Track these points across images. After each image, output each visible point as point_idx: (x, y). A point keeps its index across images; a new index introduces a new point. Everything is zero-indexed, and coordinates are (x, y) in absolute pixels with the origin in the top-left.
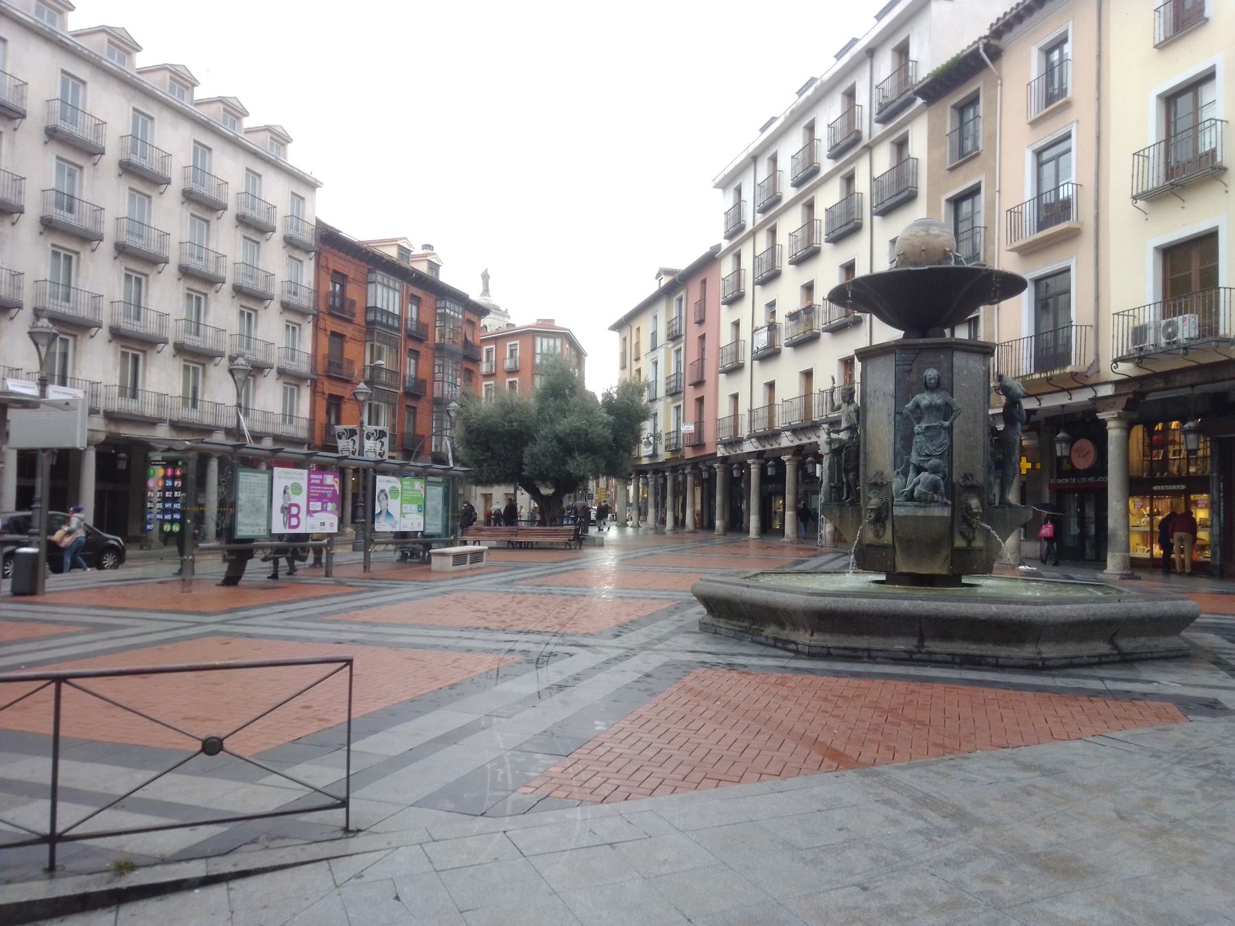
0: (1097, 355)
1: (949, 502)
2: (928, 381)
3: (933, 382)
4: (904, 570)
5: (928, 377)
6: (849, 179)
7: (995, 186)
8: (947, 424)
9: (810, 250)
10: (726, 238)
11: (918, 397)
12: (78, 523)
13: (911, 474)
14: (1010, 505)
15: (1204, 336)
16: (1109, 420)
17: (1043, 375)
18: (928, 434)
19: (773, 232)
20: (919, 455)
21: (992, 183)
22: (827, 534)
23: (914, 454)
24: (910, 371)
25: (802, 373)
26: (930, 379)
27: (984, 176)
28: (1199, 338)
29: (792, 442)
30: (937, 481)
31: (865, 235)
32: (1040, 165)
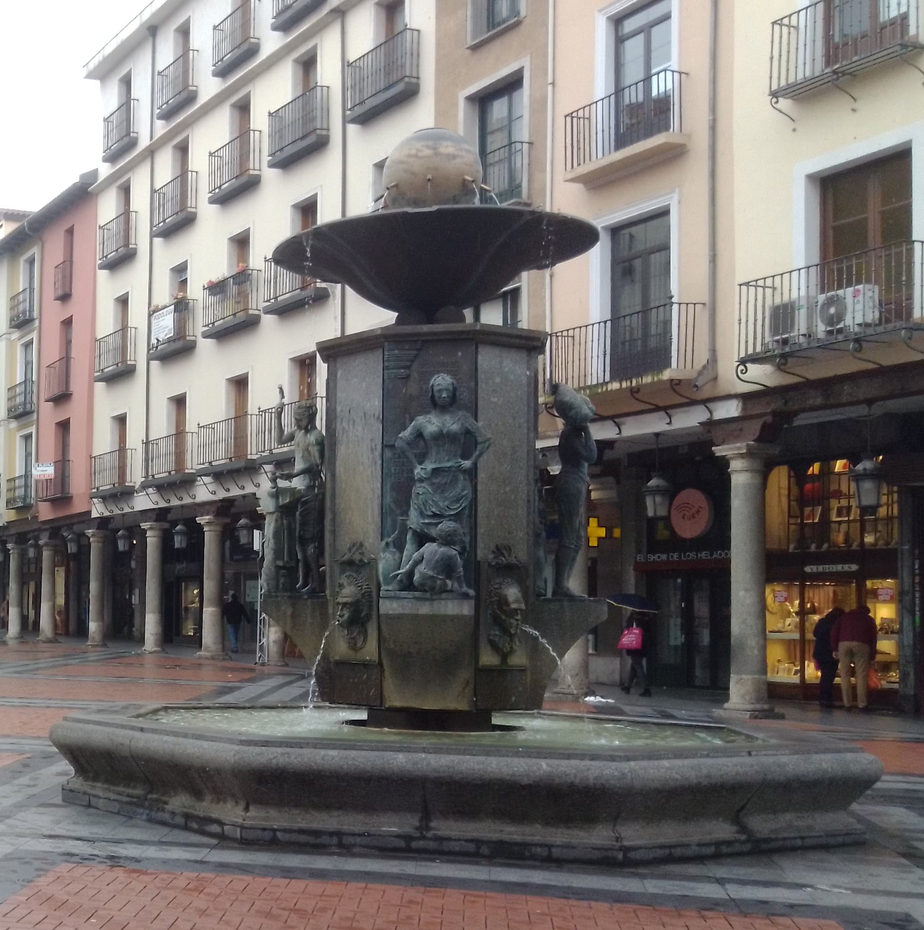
0: (713, 351)
1: (472, 592)
2: (436, 395)
4: (398, 704)
5: (436, 388)
6: (308, 64)
7: (546, 74)
8: (467, 464)
9: (244, 179)
10: (105, 160)
11: (420, 420)
13: (409, 546)
14: (571, 598)
15: (888, 321)
16: (733, 458)
17: (624, 385)
19: (183, 150)
20: (422, 515)
21: (540, 69)
22: (271, 644)
23: (413, 513)
26: (440, 391)
27: (528, 58)
29: (214, 493)
32: (620, 40)
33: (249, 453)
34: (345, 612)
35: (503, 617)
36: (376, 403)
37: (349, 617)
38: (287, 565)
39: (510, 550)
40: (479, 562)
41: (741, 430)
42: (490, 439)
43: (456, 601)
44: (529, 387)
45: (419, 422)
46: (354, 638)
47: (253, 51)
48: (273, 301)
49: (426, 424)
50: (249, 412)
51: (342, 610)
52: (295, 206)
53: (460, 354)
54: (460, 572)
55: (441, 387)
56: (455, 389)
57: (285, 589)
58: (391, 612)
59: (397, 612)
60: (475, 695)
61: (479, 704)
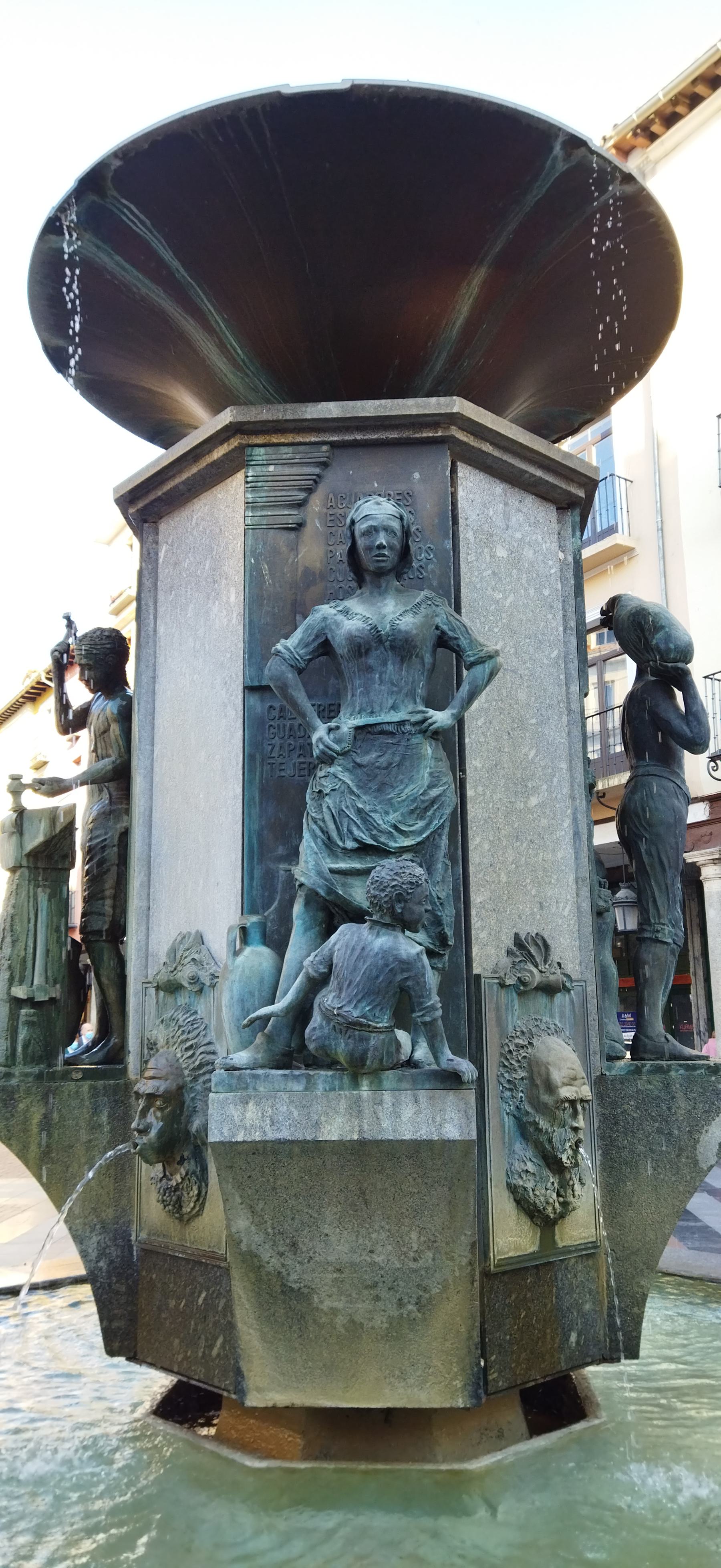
1: (466, 1067)
2: (361, 542)
3: (382, 539)
4: (280, 1398)
5: (361, 527)
8: (441, 718)
11: (326, 610)
13: (297, 941)
16: (704, 865)
20: (329, 845)
23: (308, 845)
26: (372, 531)
30: (406, 965)
34: (151, 1118)
35: (543, 1124)
36: (233, 598)
37: (161, 1133)
38: (41, 997)
39: (547, 947)
40: (478, 977)
41: (711, 834)
42: (497, 653)
43: (422, 1095)
44: (563, 579)
46: (176, 1188)
53: (417, 475)
54: (433, 1008)
55: (371, 523)
56: (406, 533)
57: (31, 1059)
59: (257, 1136)
60: (483, 1355)
61: (493, 1376)
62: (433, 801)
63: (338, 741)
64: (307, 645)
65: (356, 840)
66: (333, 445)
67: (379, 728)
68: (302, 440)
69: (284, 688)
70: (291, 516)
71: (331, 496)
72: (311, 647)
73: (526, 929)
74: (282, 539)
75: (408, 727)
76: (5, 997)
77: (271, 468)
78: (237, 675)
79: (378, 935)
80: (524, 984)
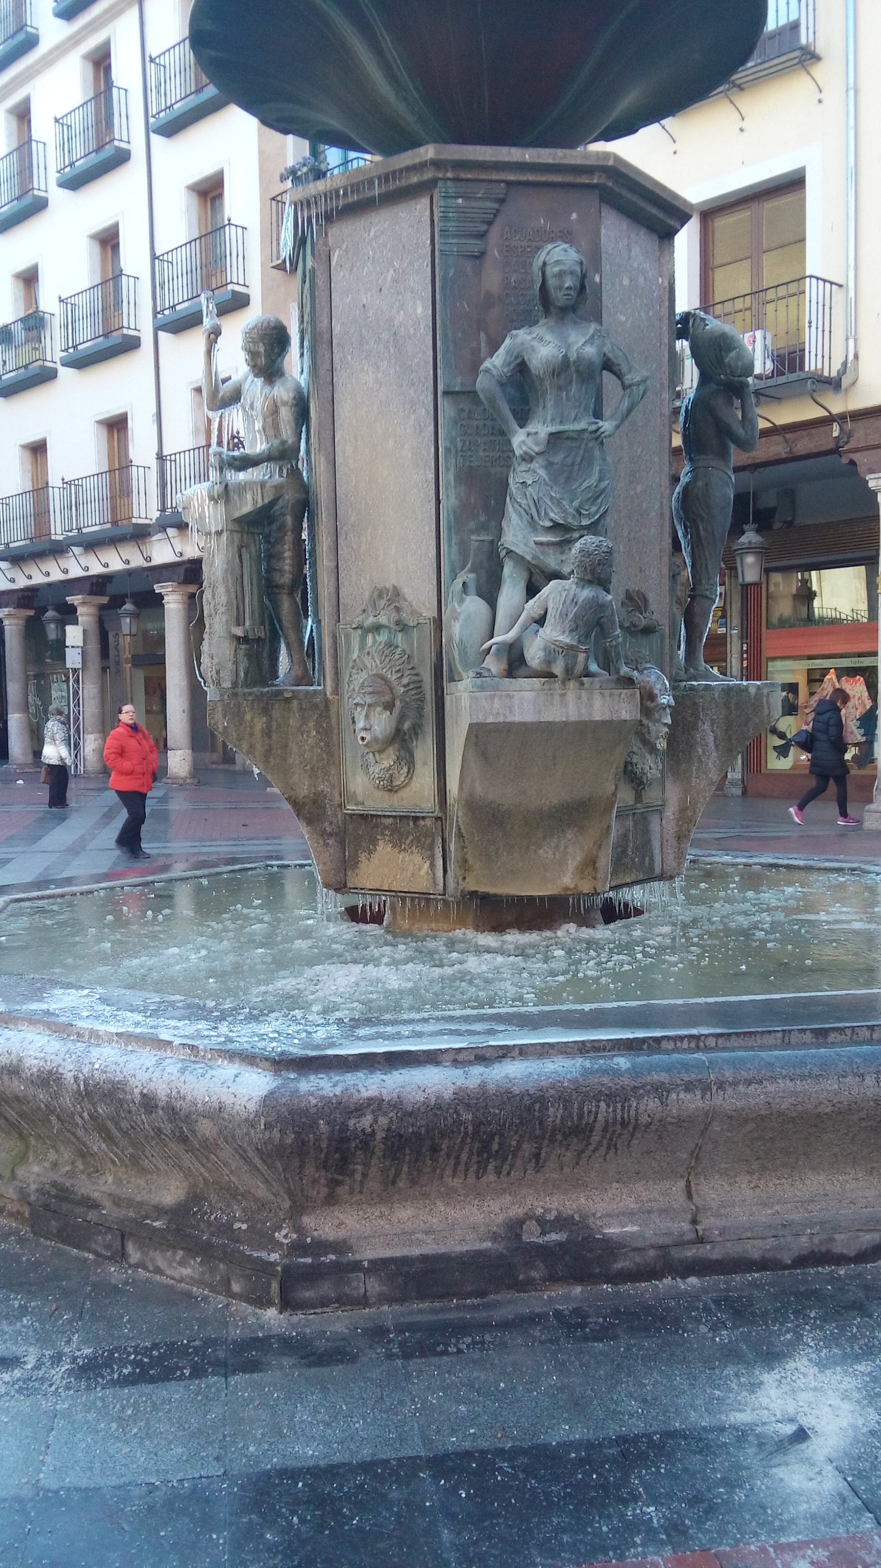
2: (552, 282)
5: (551, 270)
9: (27, 200)
11: (522, 336)
12: (471, 697)
15: (781, 373)
18: (558, 458)
20: (533, 524)
24: (482, 255)
25: (25, 447)
26: (561, 274)
28: (772, 377)
29: (13, 581)
31: (135, 169)
33: (53, 532)
36: (419, 311)
45: (518, 340)
47: (31, 43)
48: (71, 350)
49: (535, 343)
50: (50, 484)
51: (367, 717)
52: (94, 237)
55: (562, 267)
58: (490, 720)
62: (603, 491)
63: (537, 444)
64: (509, 365)
65: (551, 520)
66: (509, 183)
67: (566, 435)
68: (485, 177)
69: (492, 400)
70: (475, 246)
71: (507, 229)
72: (512, 367)
73: (633, 587)
74: (468, 266)
75: (587, 435)
76: (226, 635)
77: (460, 201)
78: (426, 378)
79: (583, 588)
80: (635, 626)
